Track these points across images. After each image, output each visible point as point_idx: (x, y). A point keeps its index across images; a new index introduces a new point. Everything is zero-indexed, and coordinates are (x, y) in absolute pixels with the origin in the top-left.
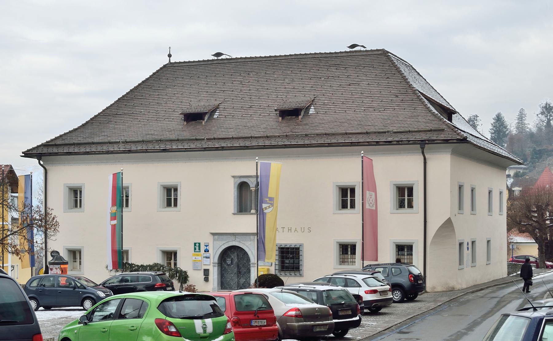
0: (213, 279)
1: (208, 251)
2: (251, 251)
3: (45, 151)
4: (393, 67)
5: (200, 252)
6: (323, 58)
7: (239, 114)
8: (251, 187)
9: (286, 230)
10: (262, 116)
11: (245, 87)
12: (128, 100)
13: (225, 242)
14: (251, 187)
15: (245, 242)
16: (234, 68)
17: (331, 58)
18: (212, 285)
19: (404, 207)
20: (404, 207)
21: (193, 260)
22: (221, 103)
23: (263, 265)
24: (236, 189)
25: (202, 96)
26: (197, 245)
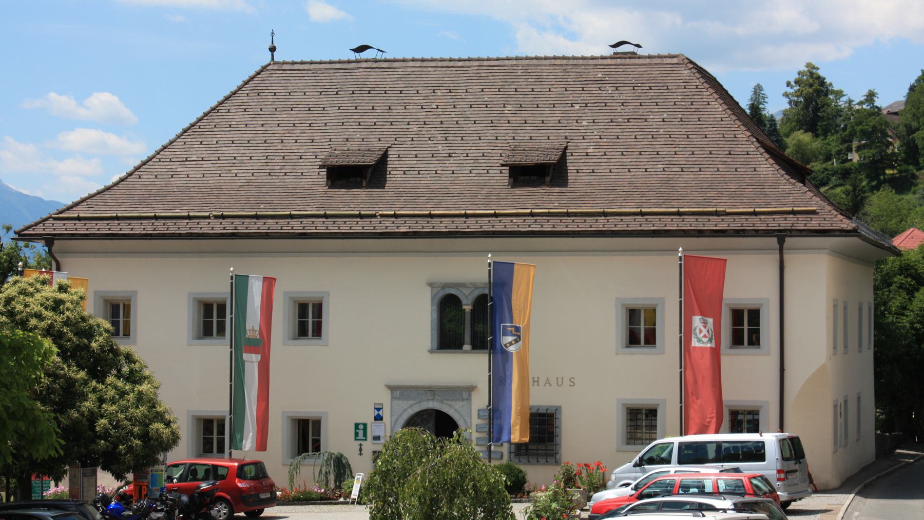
2: (464, 419)
3: (60, 228)
4: (704, 90)
6: (571, 67)
7: (430, 169)
8: (465, 305)
10: (474, 175)
11: (431, 117)
12: (203, 133)
14: (463, 303)
15: (453, 403)
16: (403, 79)
17: (586, 67)
19: (212, 335)
20: (212, 335)
22: (390, 145)
24: (435, 307)
25: (350, 130)
26: (361, 427)
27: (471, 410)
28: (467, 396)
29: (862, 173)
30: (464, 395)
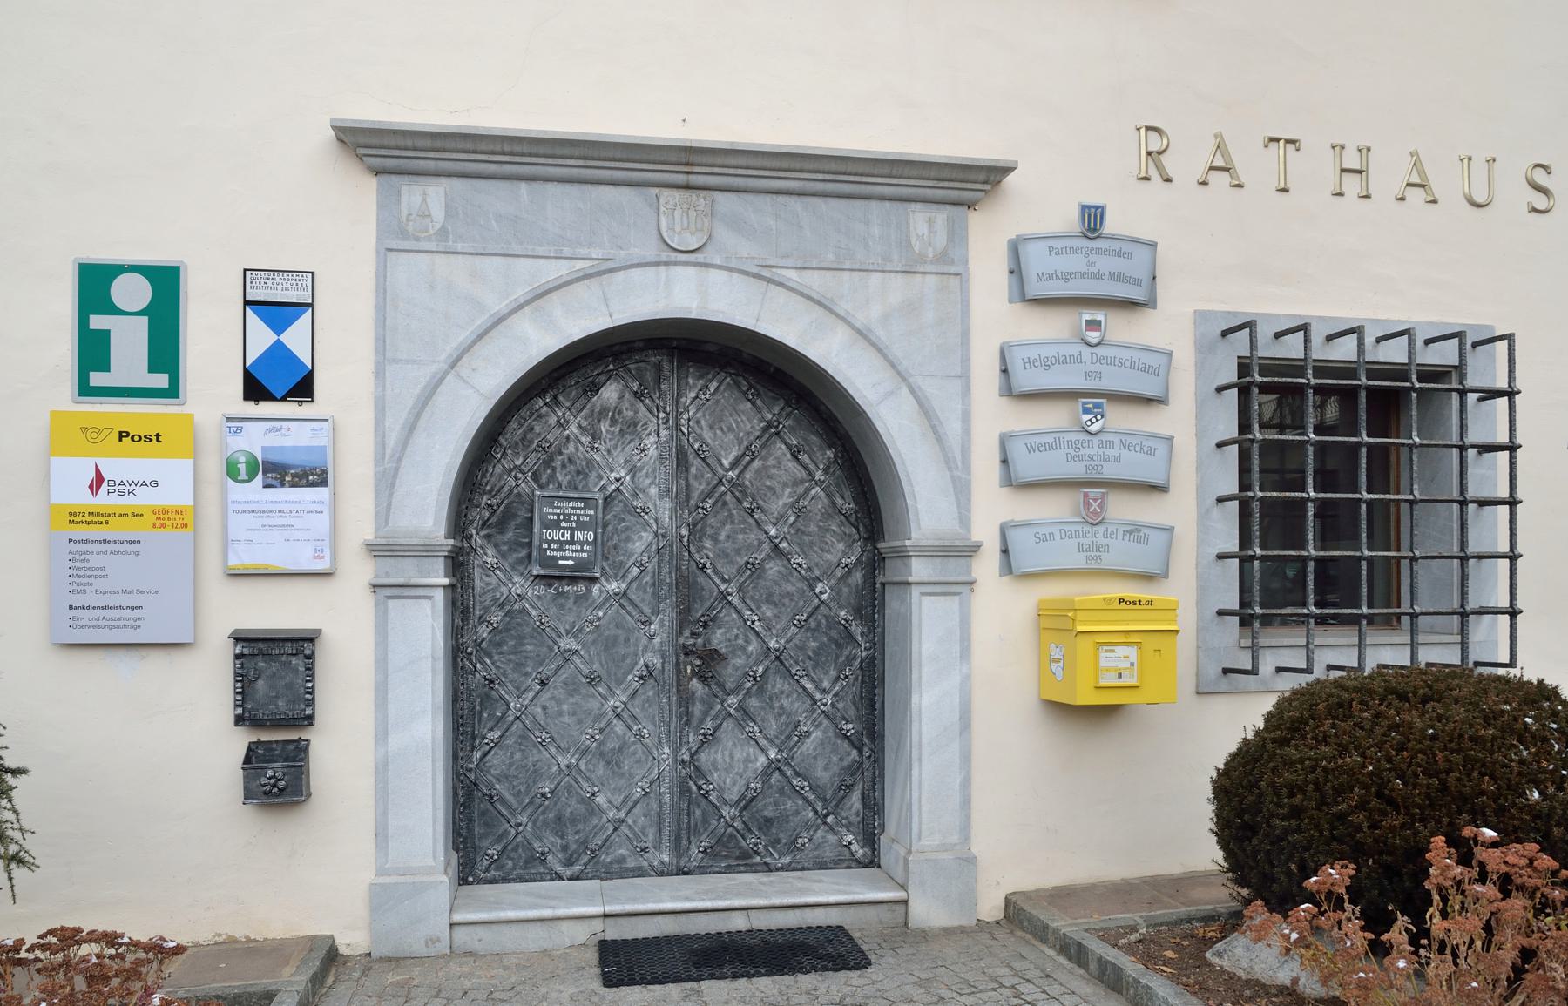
0: (382, 770)
1: (303, 389)
5: (172, 392)
9: (1388, 175)
13: (561, 269)
18: (368, 845)
21: (53, 510)
23: (1078, 561)
26: (132, 292)
27: (965, 335)
28: (941, 240)
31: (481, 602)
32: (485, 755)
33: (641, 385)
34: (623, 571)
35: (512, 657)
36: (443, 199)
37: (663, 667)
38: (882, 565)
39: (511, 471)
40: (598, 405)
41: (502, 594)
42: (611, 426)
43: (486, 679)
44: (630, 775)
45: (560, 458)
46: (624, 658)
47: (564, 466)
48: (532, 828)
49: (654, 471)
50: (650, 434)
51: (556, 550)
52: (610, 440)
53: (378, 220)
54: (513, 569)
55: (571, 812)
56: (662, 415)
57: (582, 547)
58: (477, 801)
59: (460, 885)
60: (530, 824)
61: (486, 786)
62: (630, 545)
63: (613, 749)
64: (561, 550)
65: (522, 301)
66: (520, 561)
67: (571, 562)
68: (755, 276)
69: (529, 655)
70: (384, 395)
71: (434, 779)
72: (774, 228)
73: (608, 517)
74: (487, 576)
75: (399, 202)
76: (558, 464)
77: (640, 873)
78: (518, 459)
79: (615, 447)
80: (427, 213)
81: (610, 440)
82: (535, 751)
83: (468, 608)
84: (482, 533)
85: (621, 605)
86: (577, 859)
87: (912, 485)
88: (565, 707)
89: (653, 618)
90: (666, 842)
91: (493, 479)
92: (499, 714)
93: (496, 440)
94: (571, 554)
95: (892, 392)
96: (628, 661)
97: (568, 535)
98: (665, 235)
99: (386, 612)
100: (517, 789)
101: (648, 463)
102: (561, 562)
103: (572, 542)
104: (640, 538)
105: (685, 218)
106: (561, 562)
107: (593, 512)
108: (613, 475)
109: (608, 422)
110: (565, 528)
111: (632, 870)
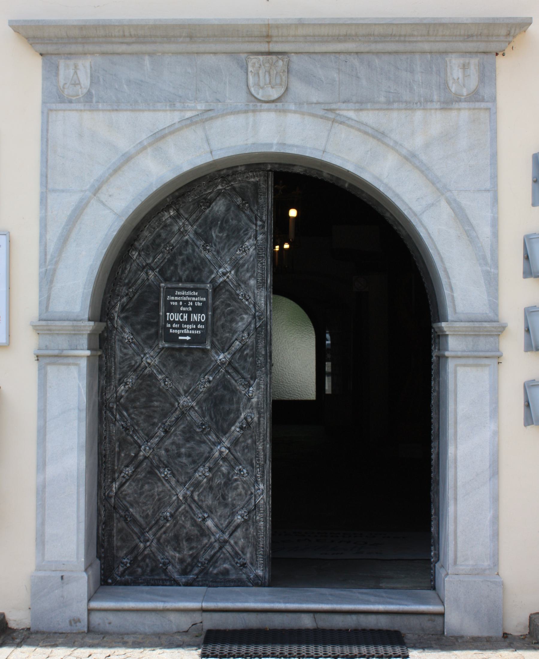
27: (494, 157)
28: (473, 82)
29: (241, 217)
30: (457, 73)
31: (121, 368)
32: (122, 485)
33: (243, 200)
34: (228, 345)
35: (143, 410)
36: (89, 71)
37: (259, 421)
38: (437, 341)
39: (144, 268)
40: (210, 215)
41: (136, 362)
42: (220, 232)
43: (123, 427)
44: (234, 506)
45: (181, 257)
46: (229, 412)
47: (183, 264)
48: (157, 544)
49: (253, 267)
50: (250, 238)
51: (177, 329)
52: (219, 243)
53: (43, 88)
54: (145, 342)
55: (187, 533)
56: (259, 223)
57: (196, 326)
58: (115, 521)
59: (101, 585)
60: (155, 541)
61: (123, 510)
62: (234, 325)
63: (219, 484)
64: (181, 328)
65: (145, 143)
66: (149, 337)
67: (188, 338)
68: (322, 117)
69: (156, 409)
70: (46, 216)
71: (78, 500)
72: (337, 79)
73: (218, 303)
74: (125, 348)
75: (57, 74)
76: (179, 262)
77: (239, 583)
78: (149, 259)
79: (223, 249)
80: (77, 82)
81: (219, 243)
82: (160, 484)
83: (110, 373)
84: (122, 315)
85: (227, 371)
86: (191, 571)
87: (449, 278)
88: (183, 450)
89: (252, 382)
90: (261, 560)
91: (131, 274)
92: (133, 454)
93: (132, 245)
94: (188, 332)
95: (433, 204)
96: (232, 415)
97: (185, 317)
98: (252, 90)
99: (46, 375)
100: (145, 514)
101: (248, 261)
102: (180, 338)
103: (189, 322)
104: (242, 319)
105: (267, 76)
106: (180, 338)
107: (205, 299)
108: (221, 270)
109: (217, 229)
110: (183, 312)
111: (233, 581)
